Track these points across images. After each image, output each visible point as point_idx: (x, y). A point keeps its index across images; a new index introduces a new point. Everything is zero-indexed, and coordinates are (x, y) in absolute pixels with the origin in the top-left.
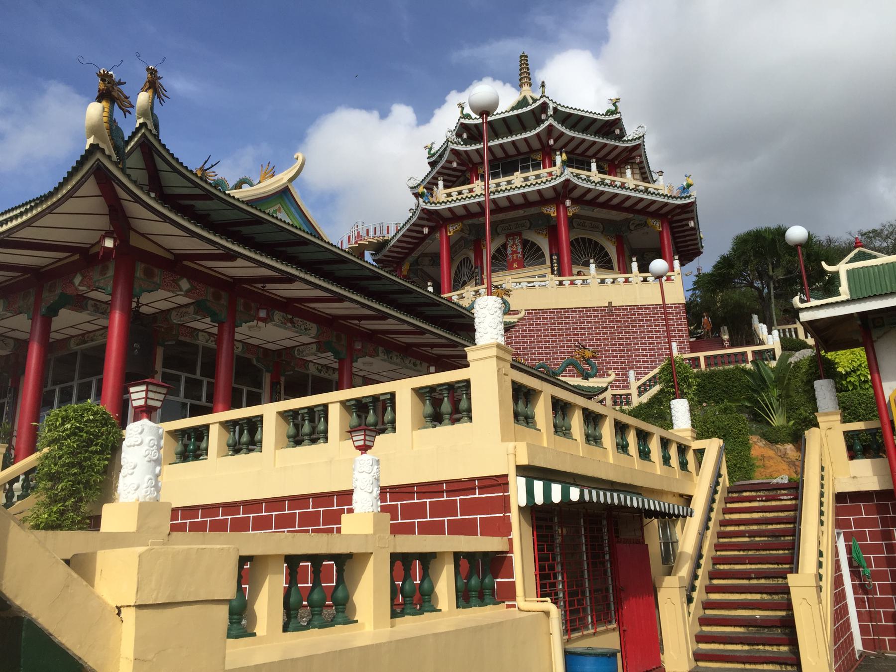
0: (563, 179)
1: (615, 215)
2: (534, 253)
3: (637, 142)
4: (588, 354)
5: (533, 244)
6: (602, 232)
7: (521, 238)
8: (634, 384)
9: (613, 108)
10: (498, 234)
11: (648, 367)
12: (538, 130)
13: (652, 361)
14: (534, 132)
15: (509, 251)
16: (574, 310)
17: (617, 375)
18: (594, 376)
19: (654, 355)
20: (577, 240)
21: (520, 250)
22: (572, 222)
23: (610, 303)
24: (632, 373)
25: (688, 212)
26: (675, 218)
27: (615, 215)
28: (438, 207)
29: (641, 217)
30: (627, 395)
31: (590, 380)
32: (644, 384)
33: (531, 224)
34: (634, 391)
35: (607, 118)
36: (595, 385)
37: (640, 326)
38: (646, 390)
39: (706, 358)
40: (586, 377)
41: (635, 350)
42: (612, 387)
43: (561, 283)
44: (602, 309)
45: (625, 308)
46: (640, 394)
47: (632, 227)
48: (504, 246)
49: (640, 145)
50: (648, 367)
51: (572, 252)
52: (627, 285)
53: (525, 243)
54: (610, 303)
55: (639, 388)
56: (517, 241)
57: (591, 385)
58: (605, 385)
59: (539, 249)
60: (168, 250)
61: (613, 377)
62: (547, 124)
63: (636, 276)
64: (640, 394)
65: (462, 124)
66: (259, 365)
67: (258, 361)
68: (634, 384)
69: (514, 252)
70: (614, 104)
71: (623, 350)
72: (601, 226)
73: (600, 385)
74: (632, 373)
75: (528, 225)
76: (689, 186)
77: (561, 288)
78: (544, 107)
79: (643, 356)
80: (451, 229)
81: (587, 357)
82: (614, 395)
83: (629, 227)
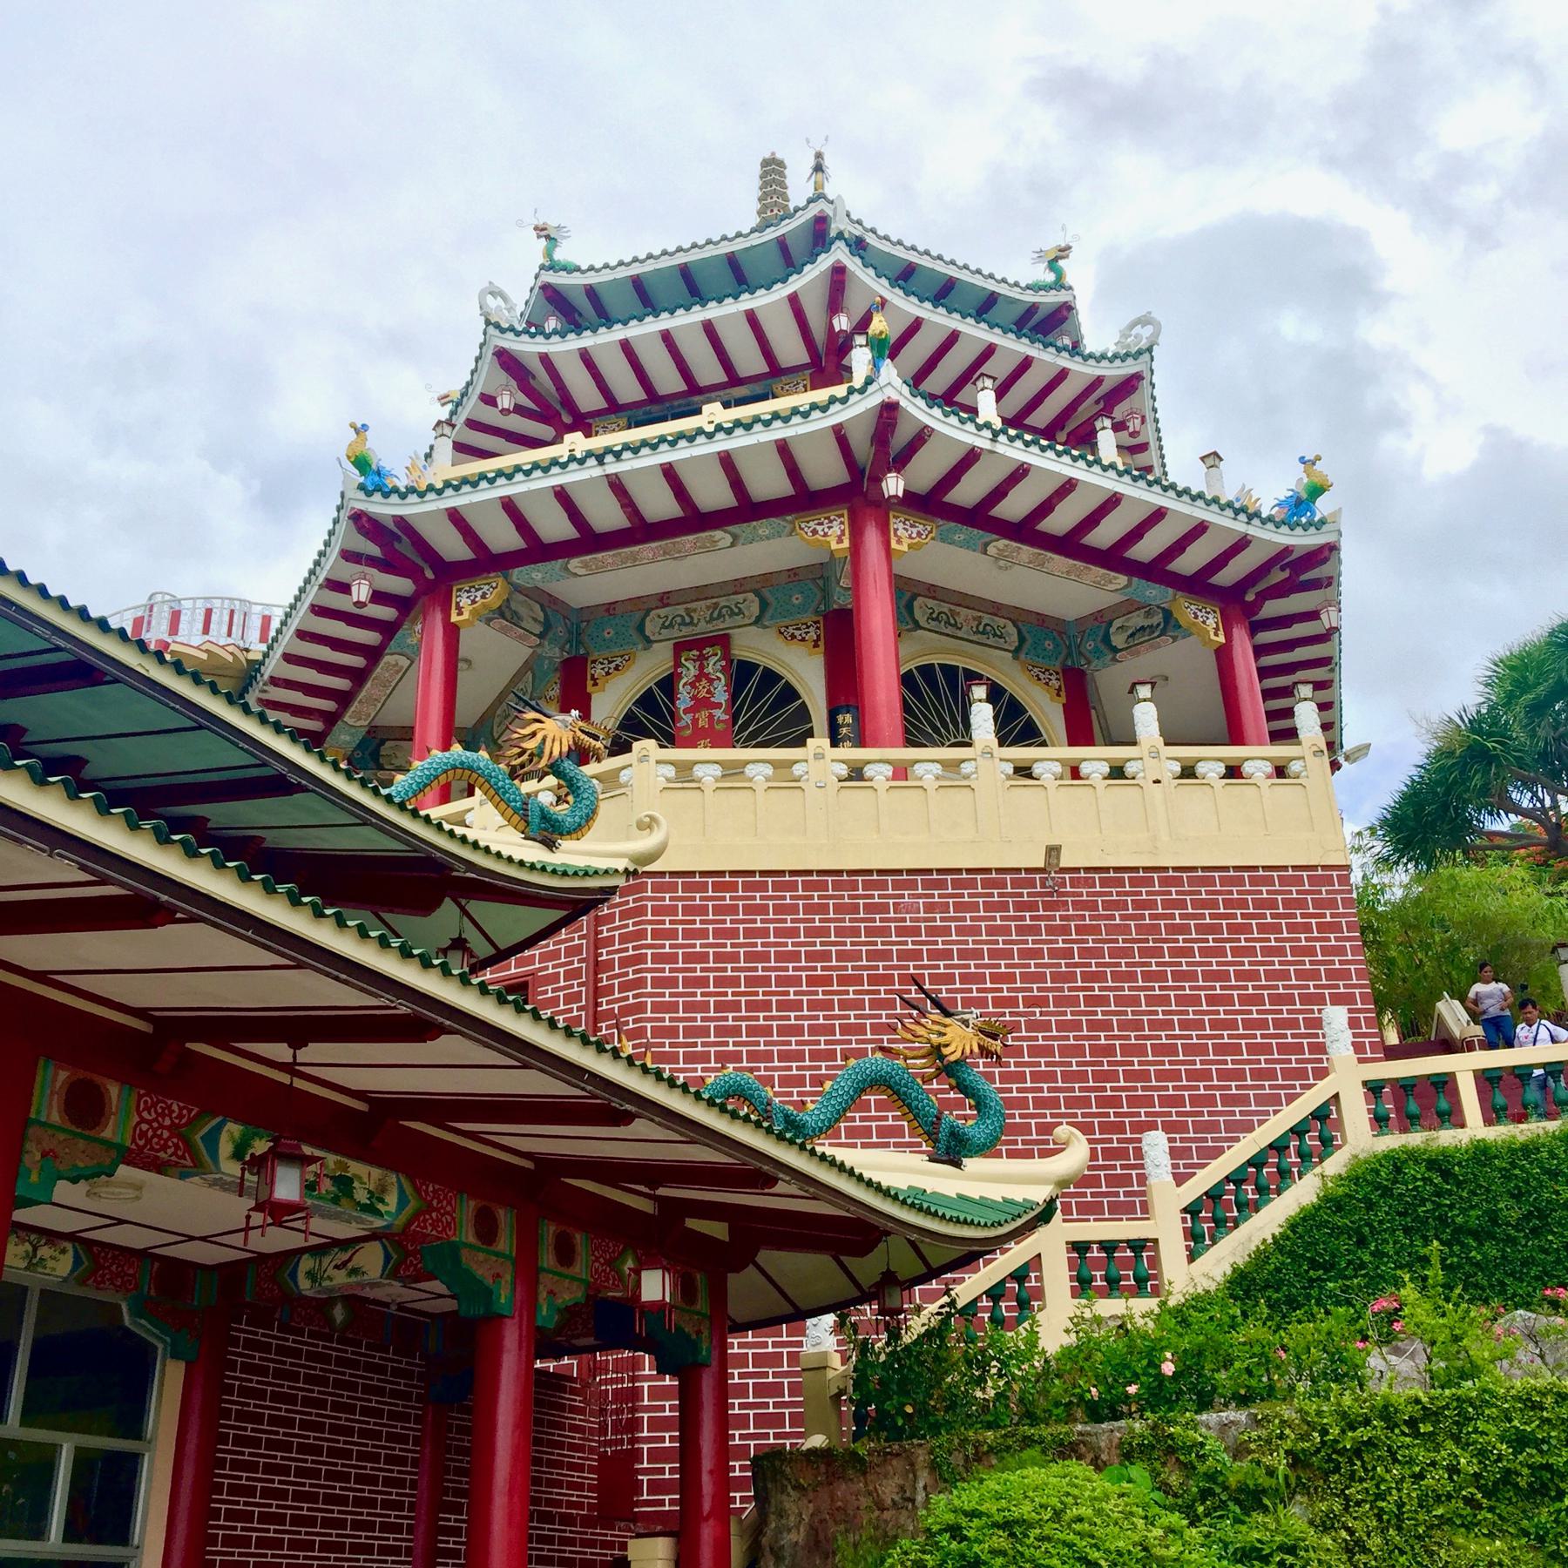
0: (873, 400)
1: (1068, 591)
2: (774, 707)
3: (1129, 368)
4: (959, 1039)
5: (771, 677)
6: (1016, 652)
7: (727, 655)
8: (1169, 1200)
9: (1050, 277)
10: (649, 642)
11: (1213, 1127)
12: (795, 284)
13: (1229, 1100)
14: (781, 292)
15: (684, 700)
16: (906, 877)
17: (1086, 1129)
18: (987, 1149)
19: (1239, 1075)
20: (927, 670)
21: (721, 696)
22: (909, 607)
23: (1053, 851)
24: (1156, 1145)
25: (1315, 585)
26: (1272, 608)
27: (1068, 591)
28: (410, 509)
29: (1154, 593)
30: (1138, 1246)
31: (972, 1164)
32: (1213, 1195)
33: (764, 605)
34: (1165, 1226)
35: (1030, 297)
36: (996, 1193)
37: (1175, 952)
38: (1222, 1225)
39: (1487, 1080)
40: (952, 1151)
41: (1159, 1050)
42: (1067, 1209)
43: (856, 773)
44: (1022, 876)
45: (1111, 875)
46: (1196, 1242)
47: (1118, 640)
48: (668, 685)
49: (1137, 377)
50: (1213, 1127)
51: (906, 708)
52: (1120, 791)
53: (742, 673)
54: (1053, 851)
55: (1192, 1210)
56: (713, 666)
57: (974, 1191)
58: (1040, 1194)
59: (790, 694)
60: (515, 1290)
61: (1075, 1155)
62: (825, 262)
63: (1155, 755)
64: (1196, 1242)
65: (546, 288)
66: (142, 1328)
67: (136, 1313)
68: (1169, 1200)
69: (701, 703)
70: (1053, 264)
71: (1108, 1051)
72: (1011, 629)
73: (1018, 1193)
74: (1156, 1145)
75: (755, 609)
76: (1317, 490)
77: (856, 796)
78: (820, 224)
79: (1193, 1075)
80: (465, 602)
81: (953, 1053)
82: (1079, 1248)
83: (1106, 639)
